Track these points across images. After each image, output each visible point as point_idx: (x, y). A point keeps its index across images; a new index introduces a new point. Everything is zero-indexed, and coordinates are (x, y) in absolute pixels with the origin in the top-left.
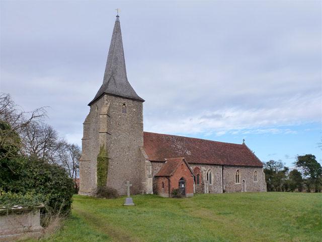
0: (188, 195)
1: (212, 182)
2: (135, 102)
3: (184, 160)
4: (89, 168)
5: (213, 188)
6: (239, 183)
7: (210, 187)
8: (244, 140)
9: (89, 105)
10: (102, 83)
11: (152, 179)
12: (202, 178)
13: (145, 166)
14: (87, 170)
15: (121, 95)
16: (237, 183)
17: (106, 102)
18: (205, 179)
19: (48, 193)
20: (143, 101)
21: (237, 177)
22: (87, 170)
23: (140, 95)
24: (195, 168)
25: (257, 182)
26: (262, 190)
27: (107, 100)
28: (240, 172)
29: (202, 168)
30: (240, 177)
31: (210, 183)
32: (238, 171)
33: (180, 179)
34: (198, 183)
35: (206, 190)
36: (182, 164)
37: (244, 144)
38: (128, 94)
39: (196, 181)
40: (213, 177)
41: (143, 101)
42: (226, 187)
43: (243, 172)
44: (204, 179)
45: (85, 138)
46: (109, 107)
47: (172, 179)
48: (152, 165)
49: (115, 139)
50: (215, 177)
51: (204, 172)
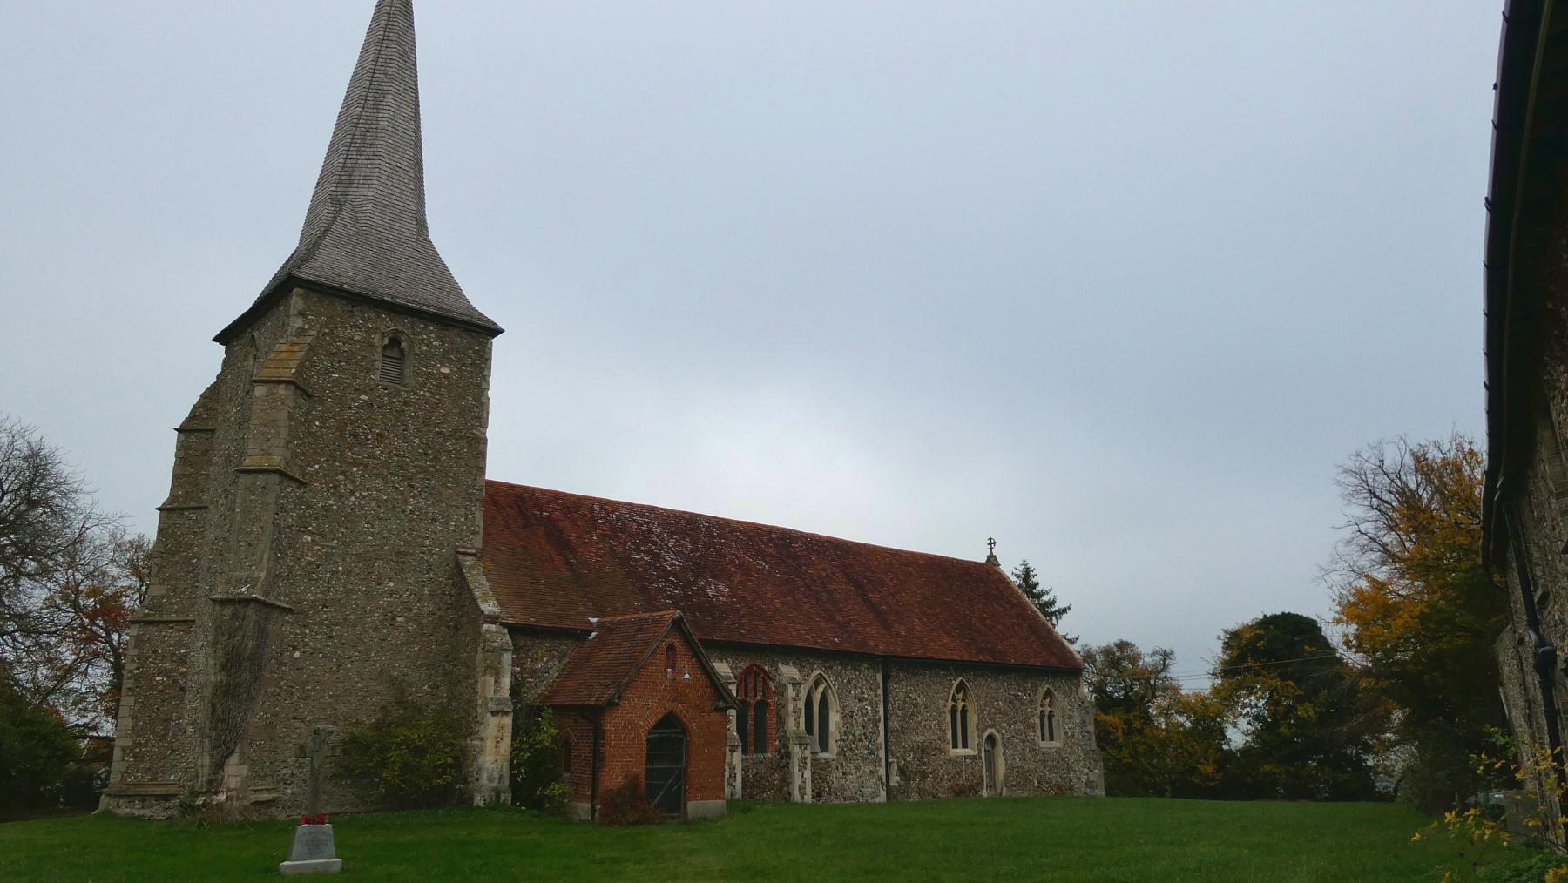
0: (694, 807)
1: (833, 745)
2: (453, 332)
3: (677, 623)
4: (183, 661)
5: (835, 776)
6: (970, 752)
7: (820, 770)
8: (992, 543)
9: (219, 339)
10: (168, 496)
11: (508, 721)
12: (781, 721)
13: (480, 656)
14: (166, 673)
15: (339, 306)
16: (960, 751)
17: (299, 323)
18: (795, 724)
19: (376, 107)
20: (500, 331)
21: (959, 718)
22: (166, 673)
23: (482, 299)
24: (747, 672)
25: (1056, 744)
26: (1081, 790)
27: (302, 314)
28: (972, 696)
29: (783, 668)
30: (973, 719)
31: (824, 747)
32: (961, 687)
33: (660, 724)
34: (760, 747)
35: (801, 780)
36: (671, 648)
37: (992, 559)
38: (424, 296)
39: (751, 739)
40: (835, 718)
41: (500, 331)
42: (902, 771)
43: (984, 697)
44: (791, 724)
45: (196, 424)
46: (311, 349)
47: (613, 724)
48: (517, 650)
49: (326, 509)
50: (848, 715)
51: (791, 693)
